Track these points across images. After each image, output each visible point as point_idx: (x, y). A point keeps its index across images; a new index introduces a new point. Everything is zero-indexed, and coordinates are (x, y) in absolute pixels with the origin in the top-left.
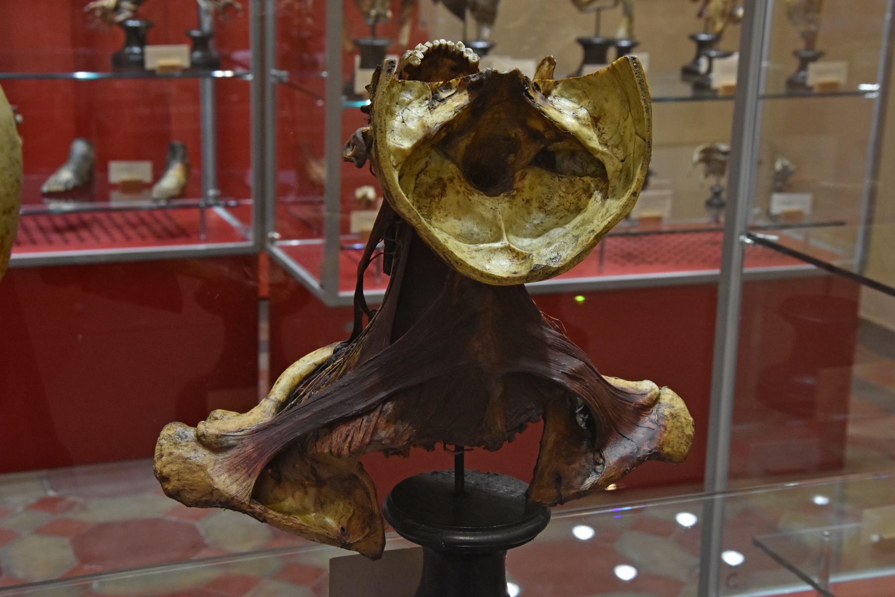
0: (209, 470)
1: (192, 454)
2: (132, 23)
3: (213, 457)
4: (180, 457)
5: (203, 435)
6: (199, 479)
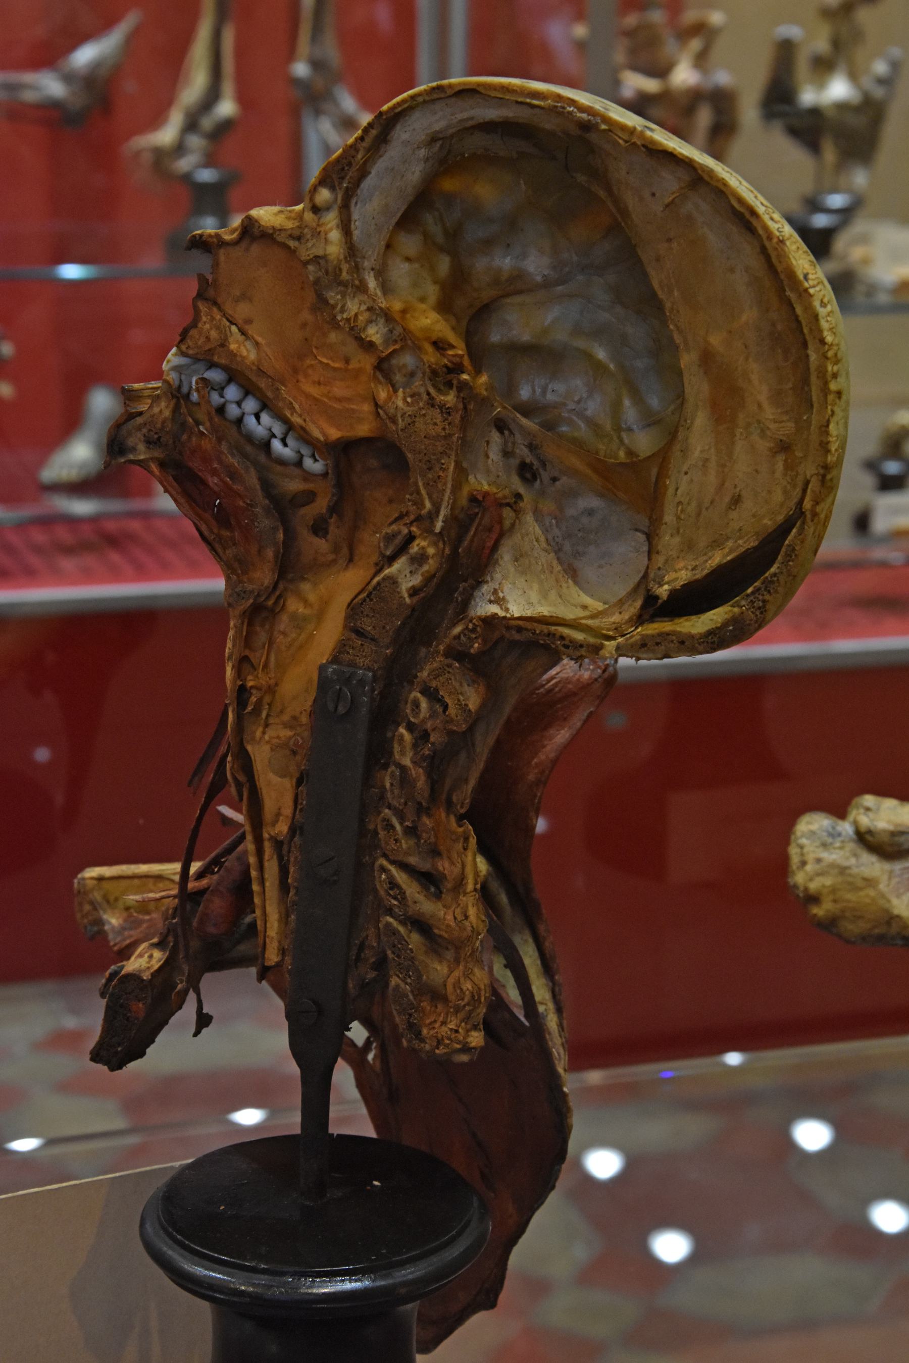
0: (882, 887)
1: (853, 861)
2: (206, 175)
3: (887, 866)
4: (833, 865)
5: (870, 832)
6: (867, 901)
